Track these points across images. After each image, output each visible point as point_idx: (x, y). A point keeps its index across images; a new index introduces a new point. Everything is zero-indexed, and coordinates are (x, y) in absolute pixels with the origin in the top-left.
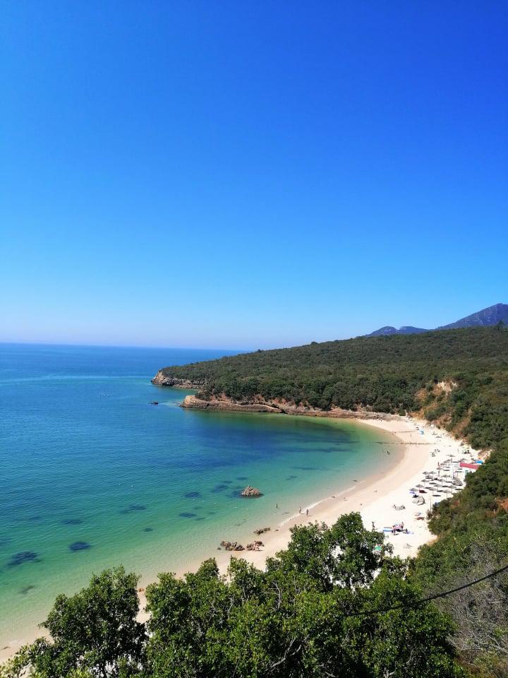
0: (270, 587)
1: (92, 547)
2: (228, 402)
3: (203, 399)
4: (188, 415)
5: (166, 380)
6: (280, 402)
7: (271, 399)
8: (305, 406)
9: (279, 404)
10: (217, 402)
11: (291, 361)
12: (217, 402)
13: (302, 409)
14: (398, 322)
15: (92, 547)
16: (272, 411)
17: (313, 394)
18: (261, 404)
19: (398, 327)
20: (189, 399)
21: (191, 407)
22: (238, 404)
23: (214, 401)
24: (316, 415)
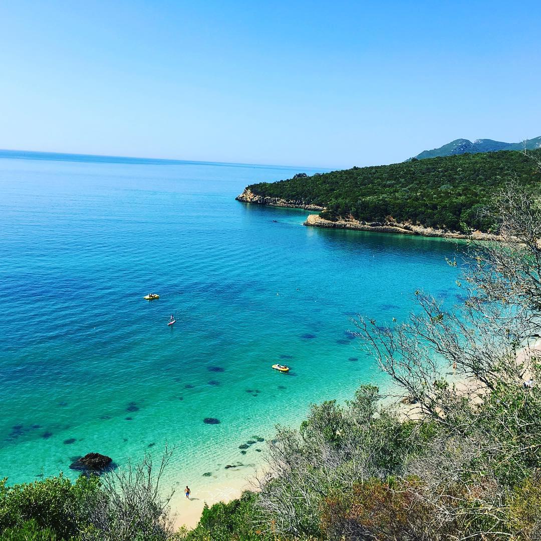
0: (111, 511)
1: (13, 428)
2: (356, 223)
3: (328, 219)
4: (311, 233)
5: (256, 198)
6: (414, 224)
7: (403, 221)
8: (442, 228)
9: (412, 227)
10: (343, 222)
11: (395, 180)
12: (343, 222)
13: (439, 232)
14: (475, 132)
15: (13, 428)
16: (405, 233)
17: (450, 216)
18: (392, 225)
19: (473, 141)
20: (313, 219)
21: (319, 226)
22: (367, 225)
23: (341, 222)
24: (453, 237)
